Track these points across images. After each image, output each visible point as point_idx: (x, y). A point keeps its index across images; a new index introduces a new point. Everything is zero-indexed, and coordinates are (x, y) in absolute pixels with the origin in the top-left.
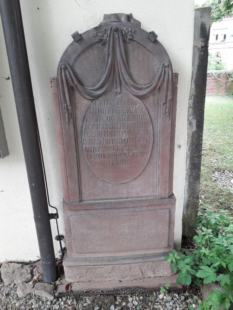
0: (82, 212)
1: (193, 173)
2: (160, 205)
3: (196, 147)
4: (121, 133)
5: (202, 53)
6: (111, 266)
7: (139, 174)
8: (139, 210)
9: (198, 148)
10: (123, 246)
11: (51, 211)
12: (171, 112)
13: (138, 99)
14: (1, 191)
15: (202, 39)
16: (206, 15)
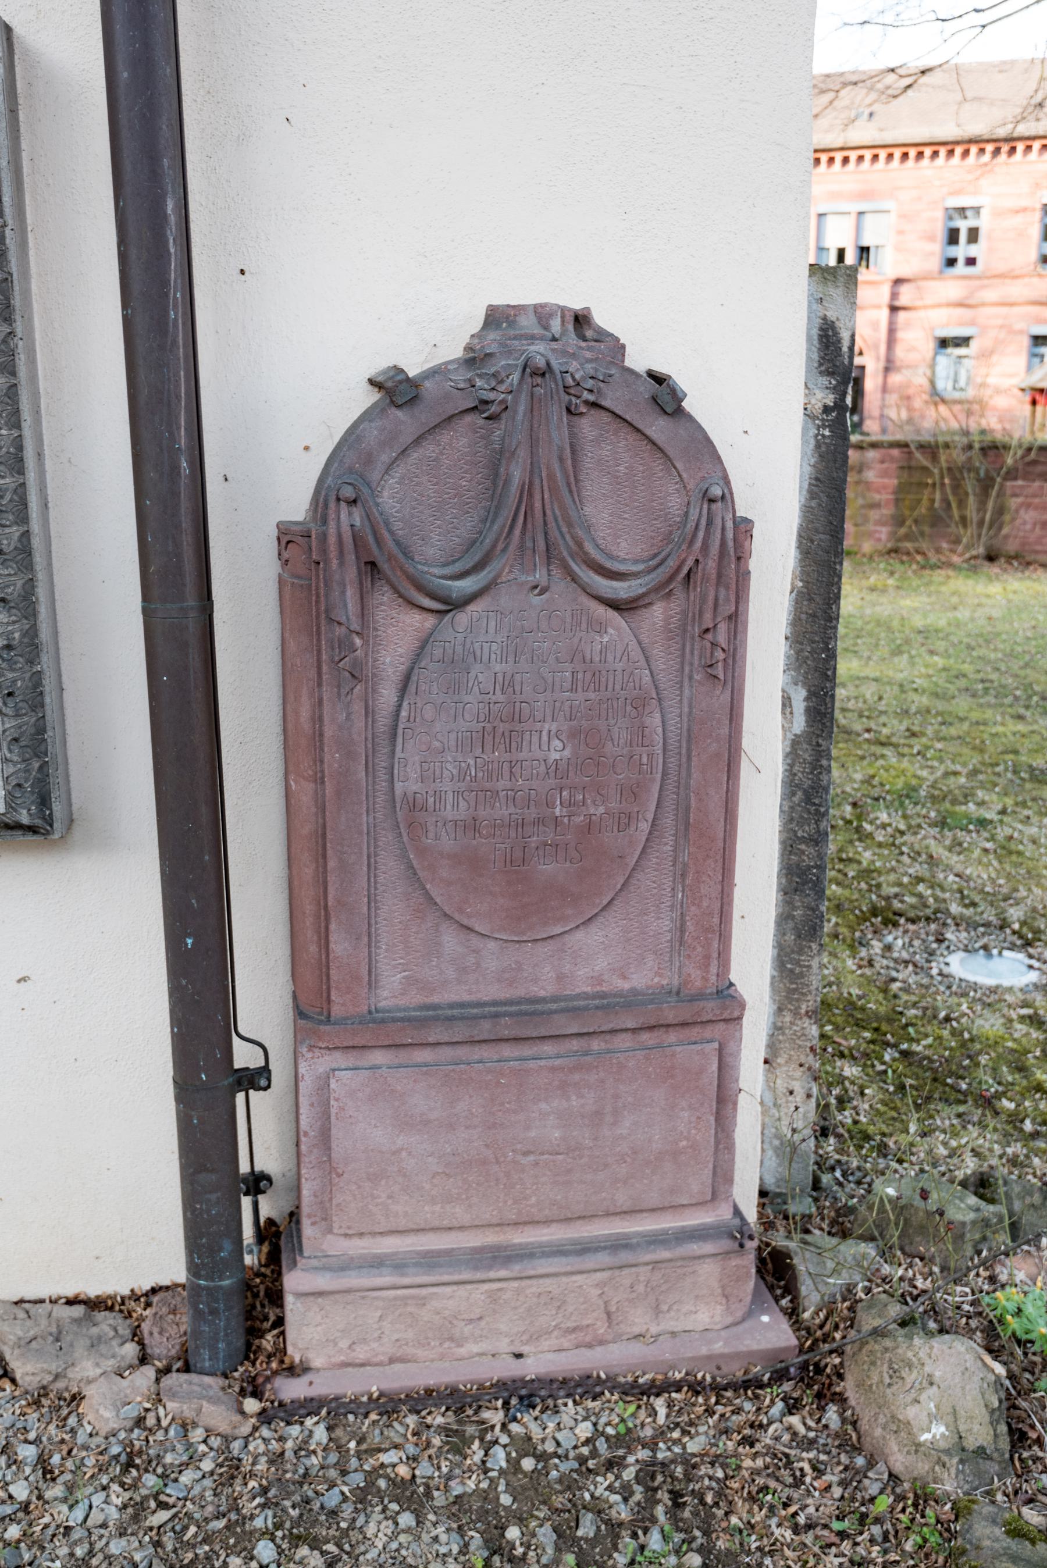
0: (379, 1057)
1: (794, 908)
2: (684, 1025)
3: (808, 799)
4: (545, 738)
5: (827, 433)
6: (486, 1287)
7: (605, 902)
8: (603, 1045)
9: (814, 804)
10: (534, 1199)
11: (244, 1056)
12: (730, 662)
13: (612, 614)
14: (19, 981)
15: (824, 381)
16: (836, 293)
